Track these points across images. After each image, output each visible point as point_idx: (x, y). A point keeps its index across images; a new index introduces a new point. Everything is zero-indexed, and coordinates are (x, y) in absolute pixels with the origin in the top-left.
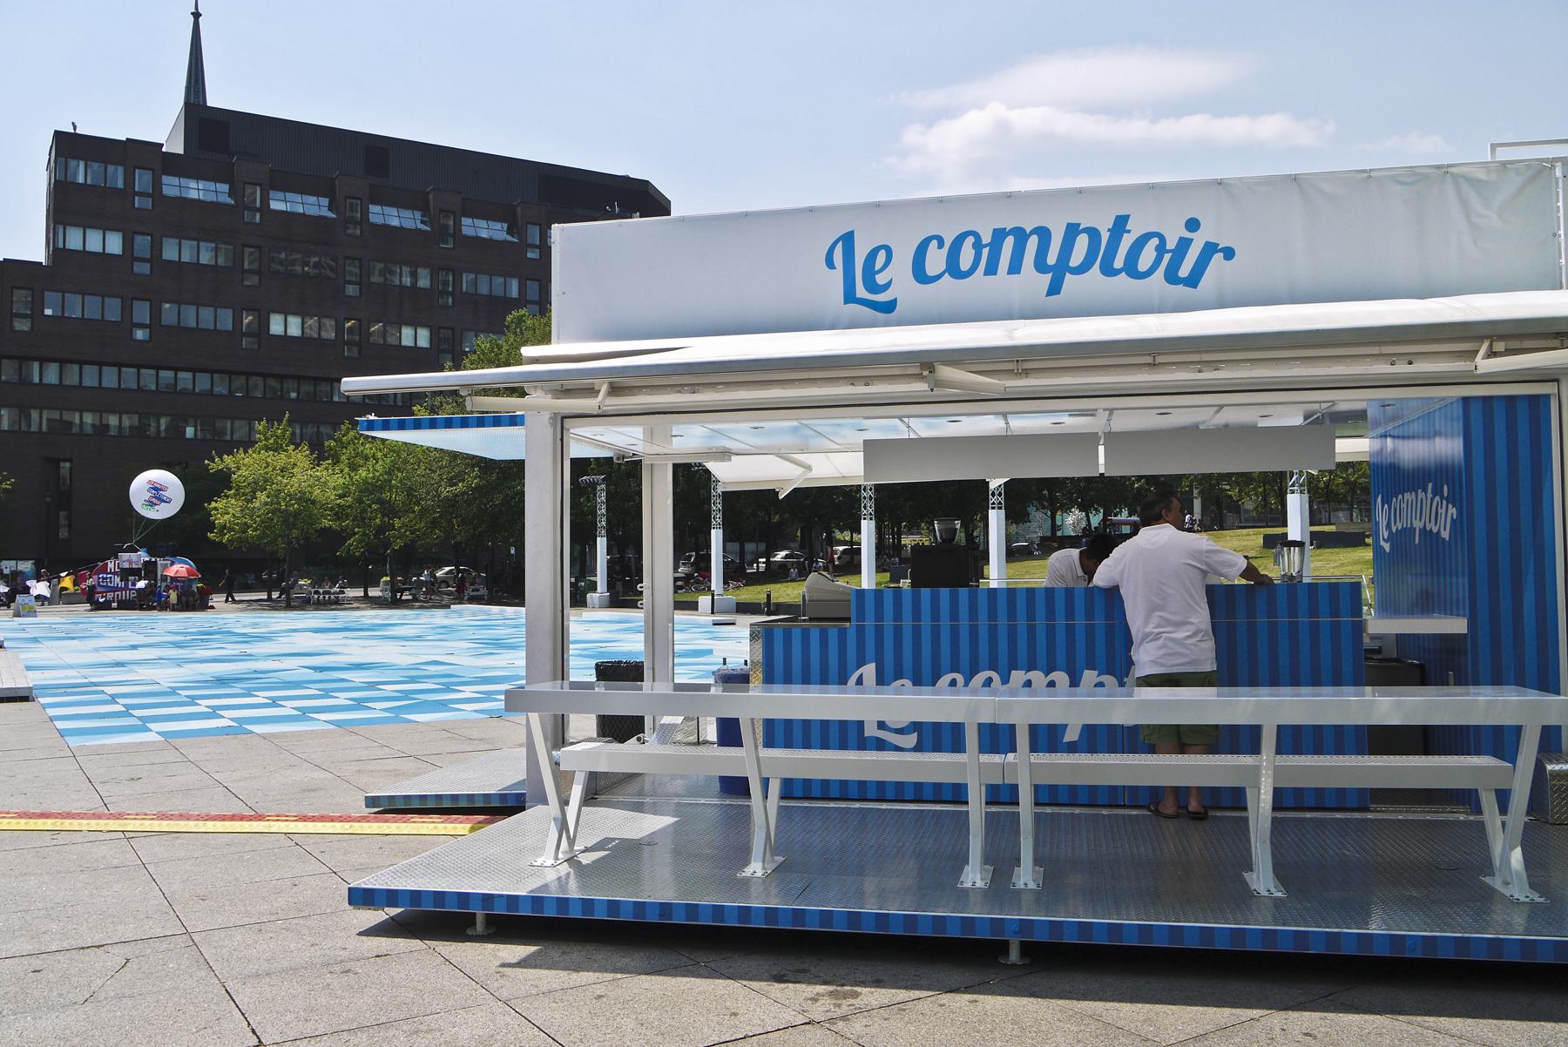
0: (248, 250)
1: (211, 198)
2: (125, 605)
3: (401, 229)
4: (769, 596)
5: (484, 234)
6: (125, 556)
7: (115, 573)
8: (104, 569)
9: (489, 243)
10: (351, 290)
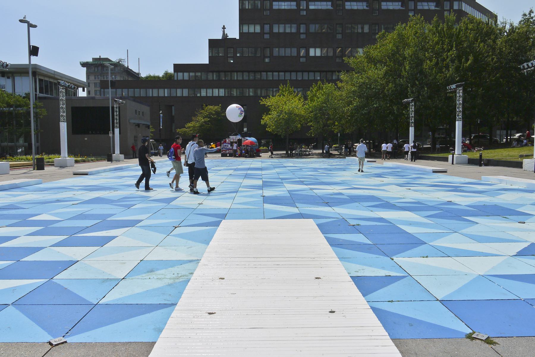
0: (301, 25)
1: (289, 8)
2: (231, 155)
3: (358, 10)
4: (481, 156)
5: (391, 8)
6: (231, 137)
7: (229, 143)
8: (225, 142)
9: (394, 10)
10: (339, 36)
